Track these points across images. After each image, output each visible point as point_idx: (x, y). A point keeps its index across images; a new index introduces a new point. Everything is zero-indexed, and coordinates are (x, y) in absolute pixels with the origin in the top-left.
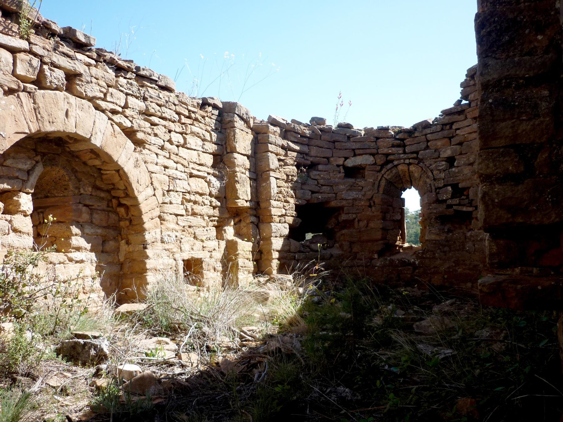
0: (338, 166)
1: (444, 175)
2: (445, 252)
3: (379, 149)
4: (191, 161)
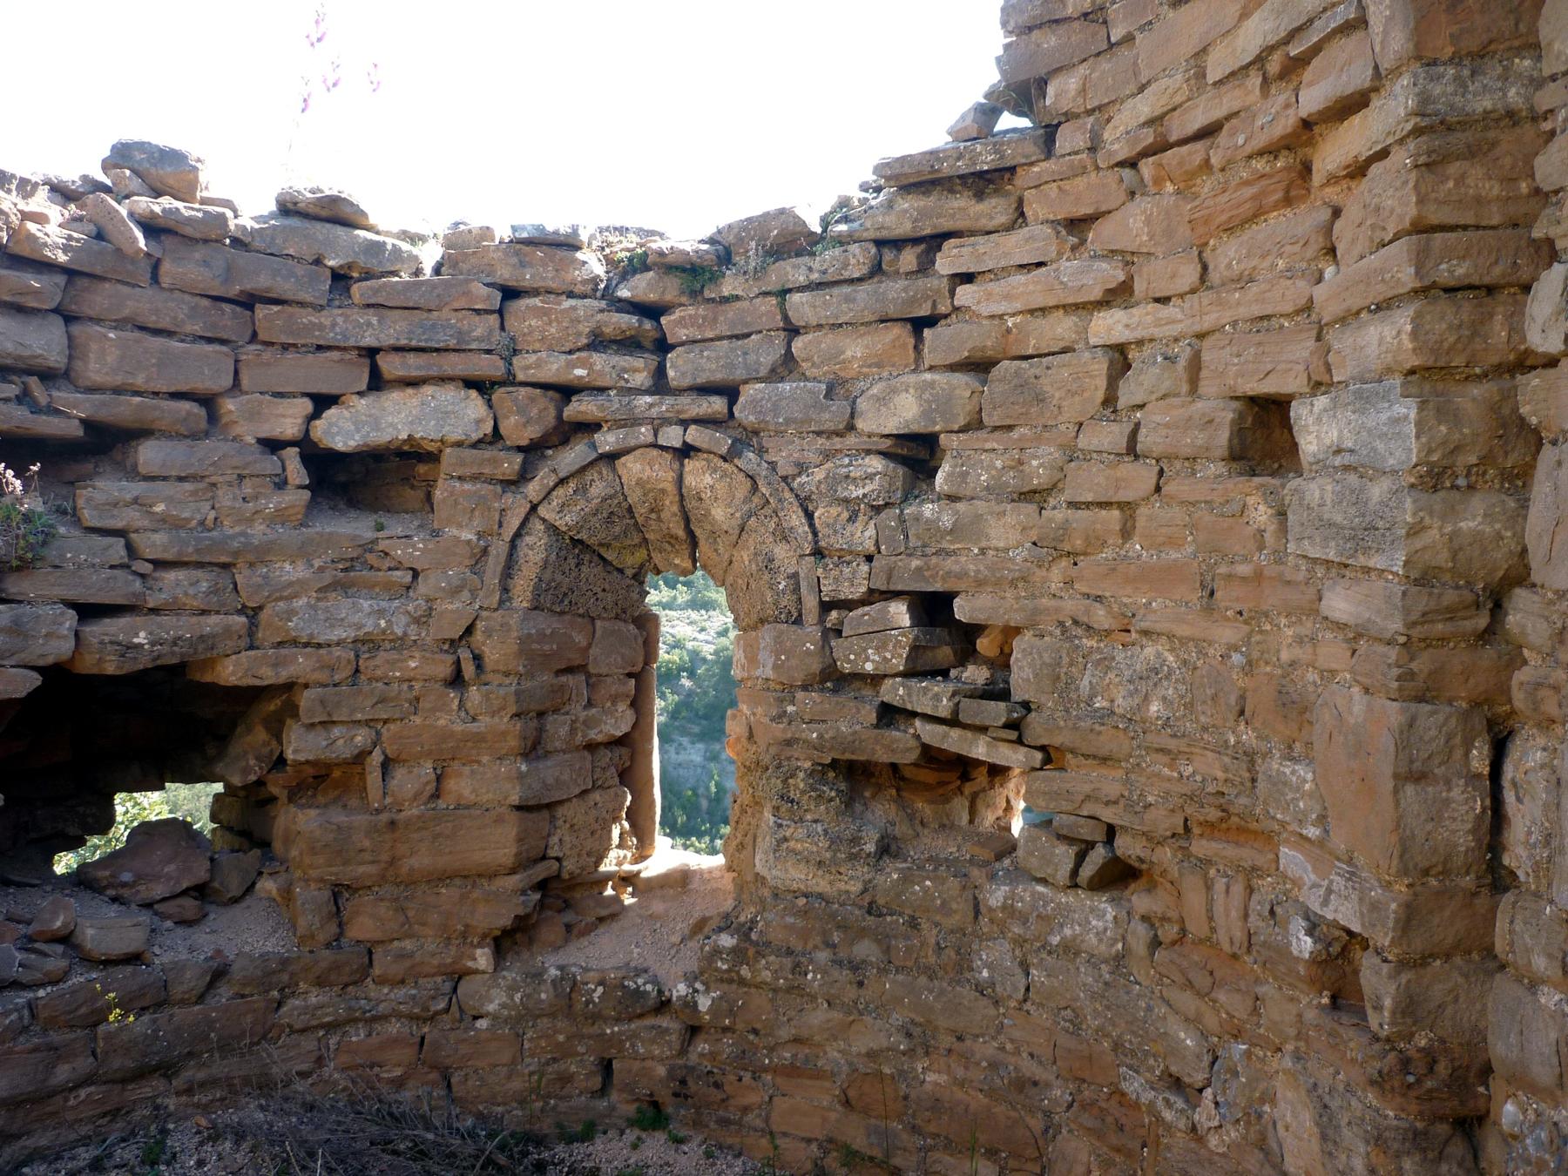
0: (273, 445)
1: (871, 532)
2: (855, 967)
3: (515, 352)
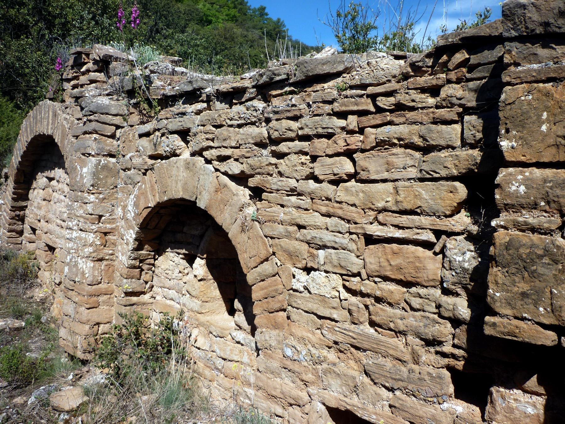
4: (373, 207)
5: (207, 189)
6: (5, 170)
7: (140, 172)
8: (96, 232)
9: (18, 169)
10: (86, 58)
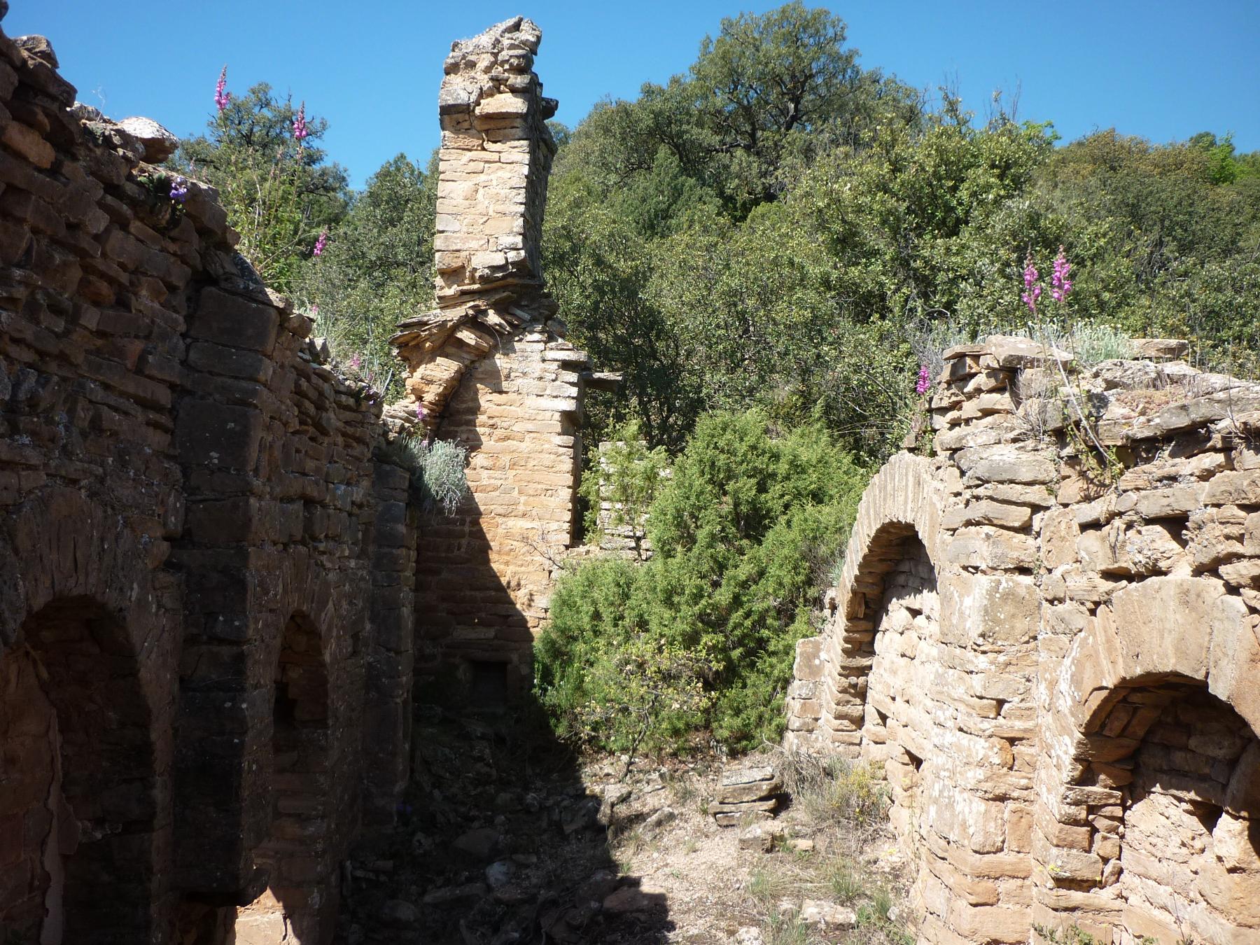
5: (1230, 653)
6: (831, 593)
7: (1083, 609)
8: (990, 736)
9: (854, 592)
10: (974, 365)
